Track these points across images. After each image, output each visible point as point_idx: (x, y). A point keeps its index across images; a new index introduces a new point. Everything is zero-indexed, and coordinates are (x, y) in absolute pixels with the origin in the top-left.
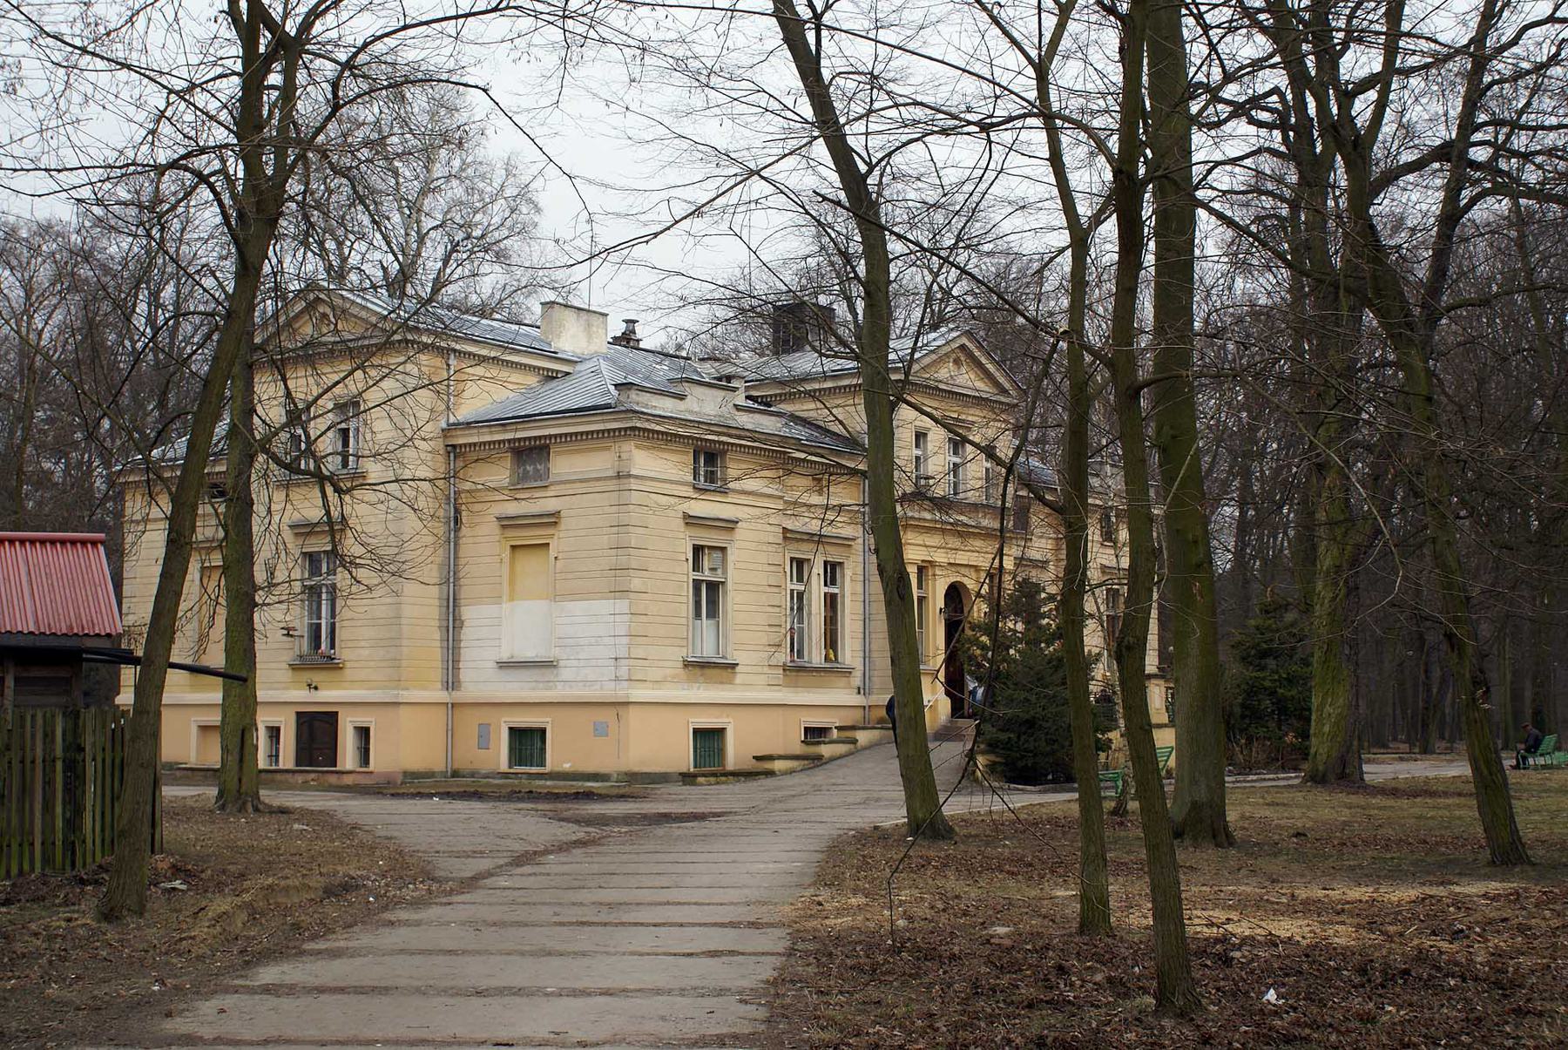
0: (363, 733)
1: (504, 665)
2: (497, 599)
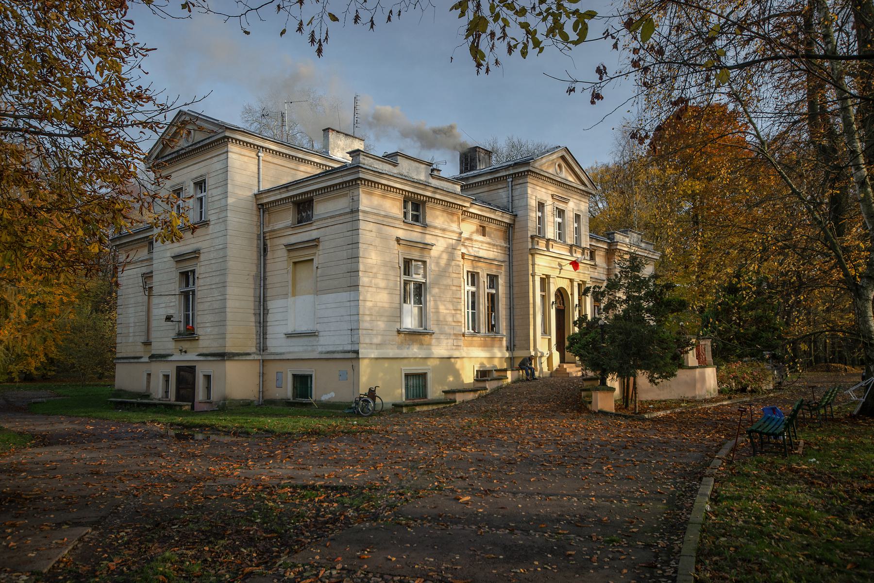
0: (208, 378)
1: (289, 336)
2: (286, 296)
